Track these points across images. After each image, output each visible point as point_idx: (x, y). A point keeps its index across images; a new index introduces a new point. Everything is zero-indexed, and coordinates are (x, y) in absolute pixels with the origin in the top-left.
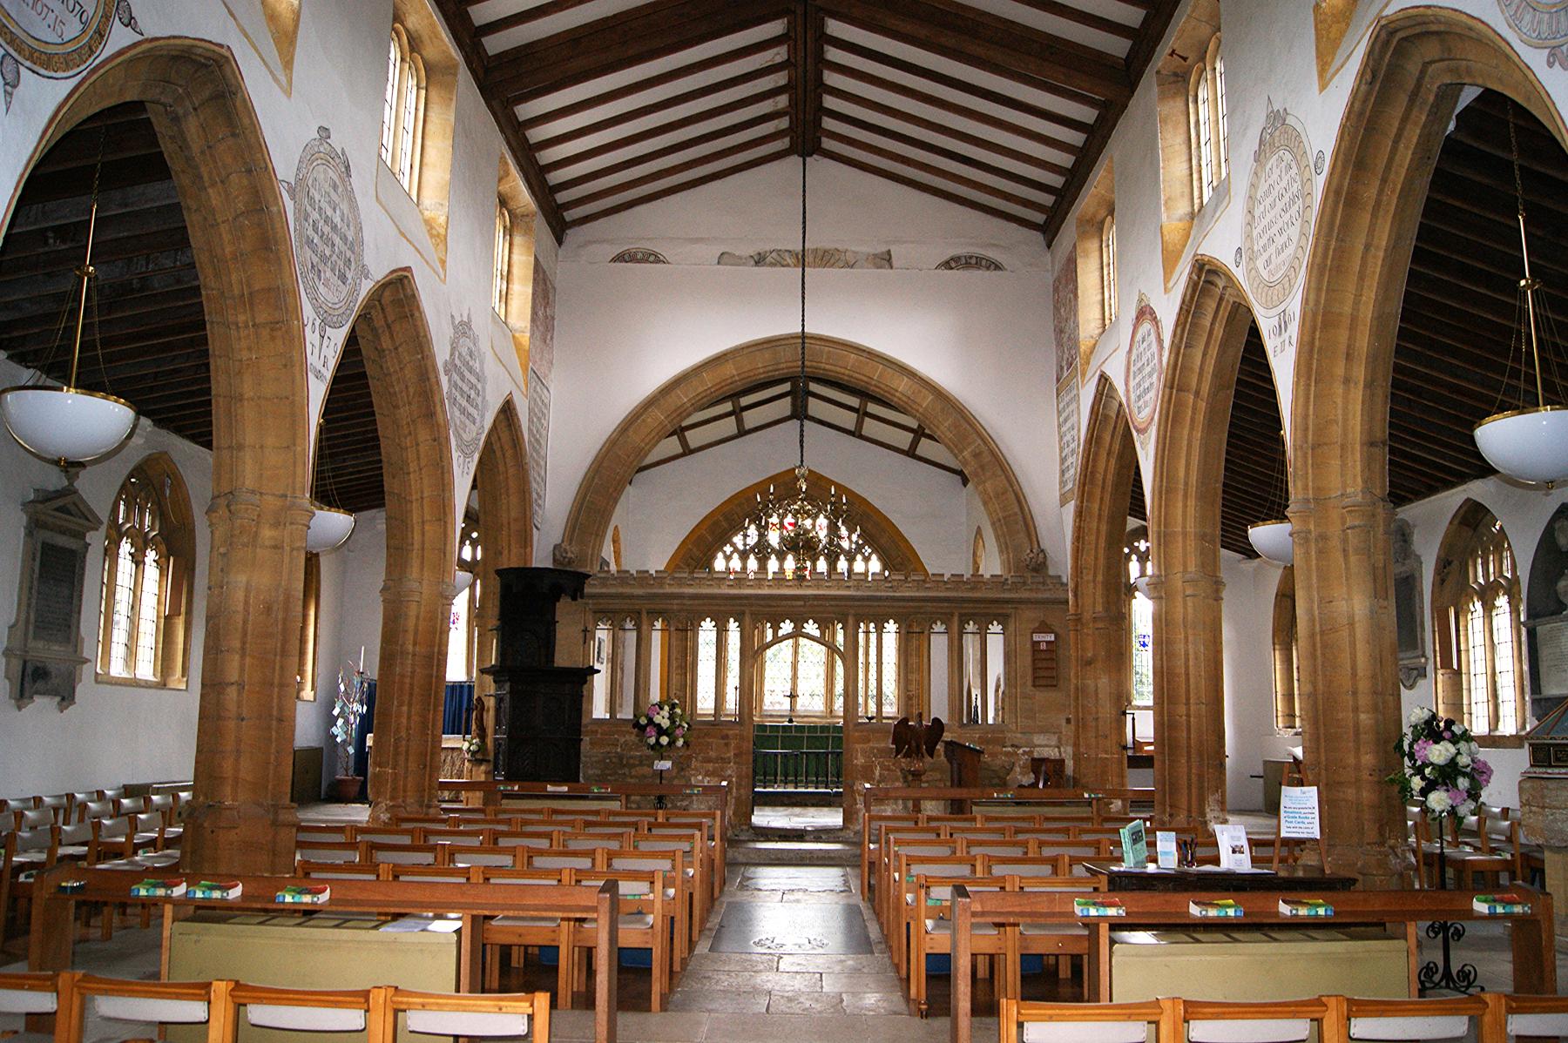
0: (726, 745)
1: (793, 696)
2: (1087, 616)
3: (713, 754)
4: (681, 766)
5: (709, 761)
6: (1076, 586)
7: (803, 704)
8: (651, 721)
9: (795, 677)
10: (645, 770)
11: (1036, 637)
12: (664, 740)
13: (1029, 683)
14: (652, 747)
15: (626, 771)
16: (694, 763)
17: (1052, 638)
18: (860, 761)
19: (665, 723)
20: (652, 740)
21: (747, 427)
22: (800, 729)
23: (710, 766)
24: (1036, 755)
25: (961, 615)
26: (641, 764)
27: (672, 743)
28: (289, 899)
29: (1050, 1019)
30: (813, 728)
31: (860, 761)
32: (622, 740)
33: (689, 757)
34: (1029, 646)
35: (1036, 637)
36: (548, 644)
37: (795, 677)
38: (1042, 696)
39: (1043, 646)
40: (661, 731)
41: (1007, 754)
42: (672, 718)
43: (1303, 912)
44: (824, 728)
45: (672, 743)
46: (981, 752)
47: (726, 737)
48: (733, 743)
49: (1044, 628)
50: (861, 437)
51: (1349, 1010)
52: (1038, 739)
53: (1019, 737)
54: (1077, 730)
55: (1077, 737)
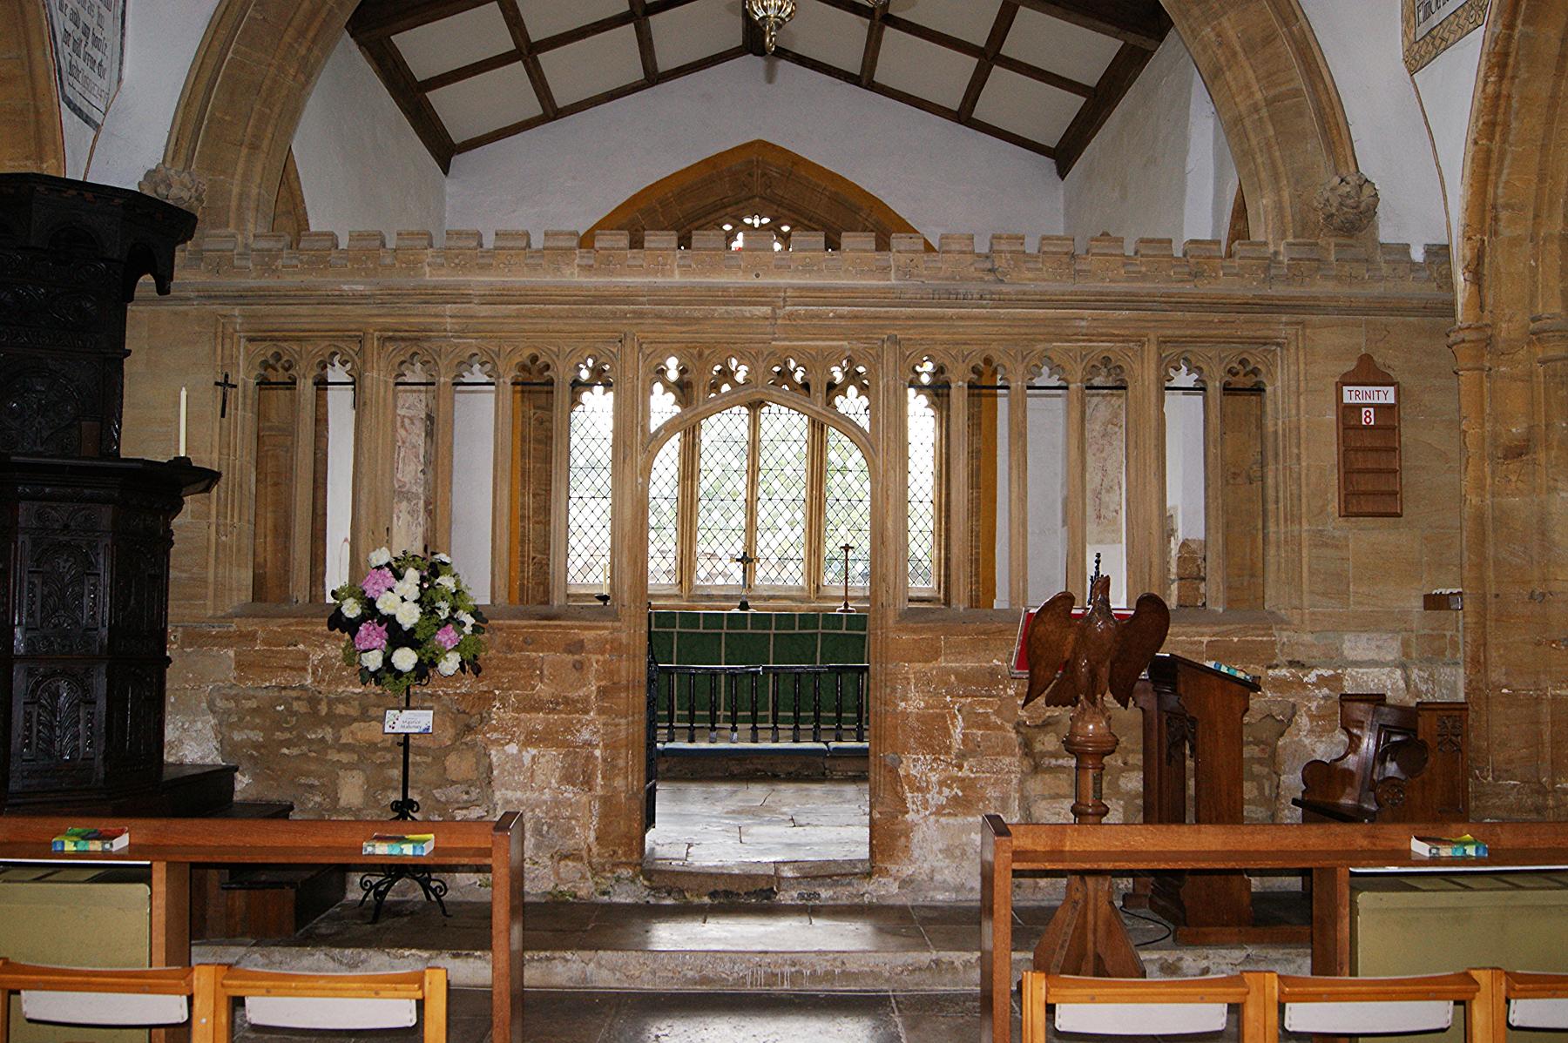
0: (579, 666)
1: (747, 560)
2: (1506, 330)
3: (543, 689)
4: (466, 722)
5: (534, 705)
6: (1479, 257)
7: (764, 574)
8: (370, 605)
9: (751, 528)
10: (361, 732)
11: (1350, 395)
12: (405, 659)
13: (1333, 506)
14: (376, 676)
15: (328, 733)
16: (497, 713)
17: (1387, 396)
18: (914, 703)
19: (409, 616)
20: (373, 661)
21: (662, 68)
22: (762, 620)
23: (538, 720)
24: (1349, 688)
25: (1163, 342)
26: (364, 716)
27: (424, 669)
28: (69, 847)
29: (1093, 1000)
30: (786, 620)
31: (914, 703)
32: (316, 656)
33: (486, 699)
34: (1331, 417)
35: (1350, 395)
36: (105, 401)
37: (751, 528)
38: (1368, 537)
39: (1368, 418)
40: (398, 636)
41: (1279, 684)
42: (426, 602)
43: (1446, 851)
44: (808, 620)
45: (424, 669)
46: (1254, 686)
47: (577, 647)
48: (595, 661)
49: (1368, 373)
50: (872, 86)
51: (1510, 989)
52: (1356, 646)
53: (1305, 640)
54: (1482, 624)
55: (1482, 644)
